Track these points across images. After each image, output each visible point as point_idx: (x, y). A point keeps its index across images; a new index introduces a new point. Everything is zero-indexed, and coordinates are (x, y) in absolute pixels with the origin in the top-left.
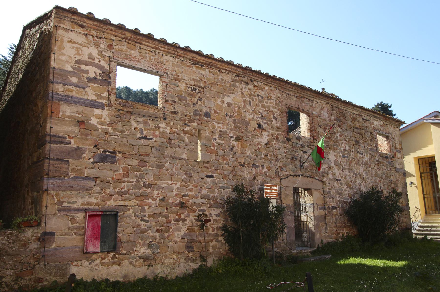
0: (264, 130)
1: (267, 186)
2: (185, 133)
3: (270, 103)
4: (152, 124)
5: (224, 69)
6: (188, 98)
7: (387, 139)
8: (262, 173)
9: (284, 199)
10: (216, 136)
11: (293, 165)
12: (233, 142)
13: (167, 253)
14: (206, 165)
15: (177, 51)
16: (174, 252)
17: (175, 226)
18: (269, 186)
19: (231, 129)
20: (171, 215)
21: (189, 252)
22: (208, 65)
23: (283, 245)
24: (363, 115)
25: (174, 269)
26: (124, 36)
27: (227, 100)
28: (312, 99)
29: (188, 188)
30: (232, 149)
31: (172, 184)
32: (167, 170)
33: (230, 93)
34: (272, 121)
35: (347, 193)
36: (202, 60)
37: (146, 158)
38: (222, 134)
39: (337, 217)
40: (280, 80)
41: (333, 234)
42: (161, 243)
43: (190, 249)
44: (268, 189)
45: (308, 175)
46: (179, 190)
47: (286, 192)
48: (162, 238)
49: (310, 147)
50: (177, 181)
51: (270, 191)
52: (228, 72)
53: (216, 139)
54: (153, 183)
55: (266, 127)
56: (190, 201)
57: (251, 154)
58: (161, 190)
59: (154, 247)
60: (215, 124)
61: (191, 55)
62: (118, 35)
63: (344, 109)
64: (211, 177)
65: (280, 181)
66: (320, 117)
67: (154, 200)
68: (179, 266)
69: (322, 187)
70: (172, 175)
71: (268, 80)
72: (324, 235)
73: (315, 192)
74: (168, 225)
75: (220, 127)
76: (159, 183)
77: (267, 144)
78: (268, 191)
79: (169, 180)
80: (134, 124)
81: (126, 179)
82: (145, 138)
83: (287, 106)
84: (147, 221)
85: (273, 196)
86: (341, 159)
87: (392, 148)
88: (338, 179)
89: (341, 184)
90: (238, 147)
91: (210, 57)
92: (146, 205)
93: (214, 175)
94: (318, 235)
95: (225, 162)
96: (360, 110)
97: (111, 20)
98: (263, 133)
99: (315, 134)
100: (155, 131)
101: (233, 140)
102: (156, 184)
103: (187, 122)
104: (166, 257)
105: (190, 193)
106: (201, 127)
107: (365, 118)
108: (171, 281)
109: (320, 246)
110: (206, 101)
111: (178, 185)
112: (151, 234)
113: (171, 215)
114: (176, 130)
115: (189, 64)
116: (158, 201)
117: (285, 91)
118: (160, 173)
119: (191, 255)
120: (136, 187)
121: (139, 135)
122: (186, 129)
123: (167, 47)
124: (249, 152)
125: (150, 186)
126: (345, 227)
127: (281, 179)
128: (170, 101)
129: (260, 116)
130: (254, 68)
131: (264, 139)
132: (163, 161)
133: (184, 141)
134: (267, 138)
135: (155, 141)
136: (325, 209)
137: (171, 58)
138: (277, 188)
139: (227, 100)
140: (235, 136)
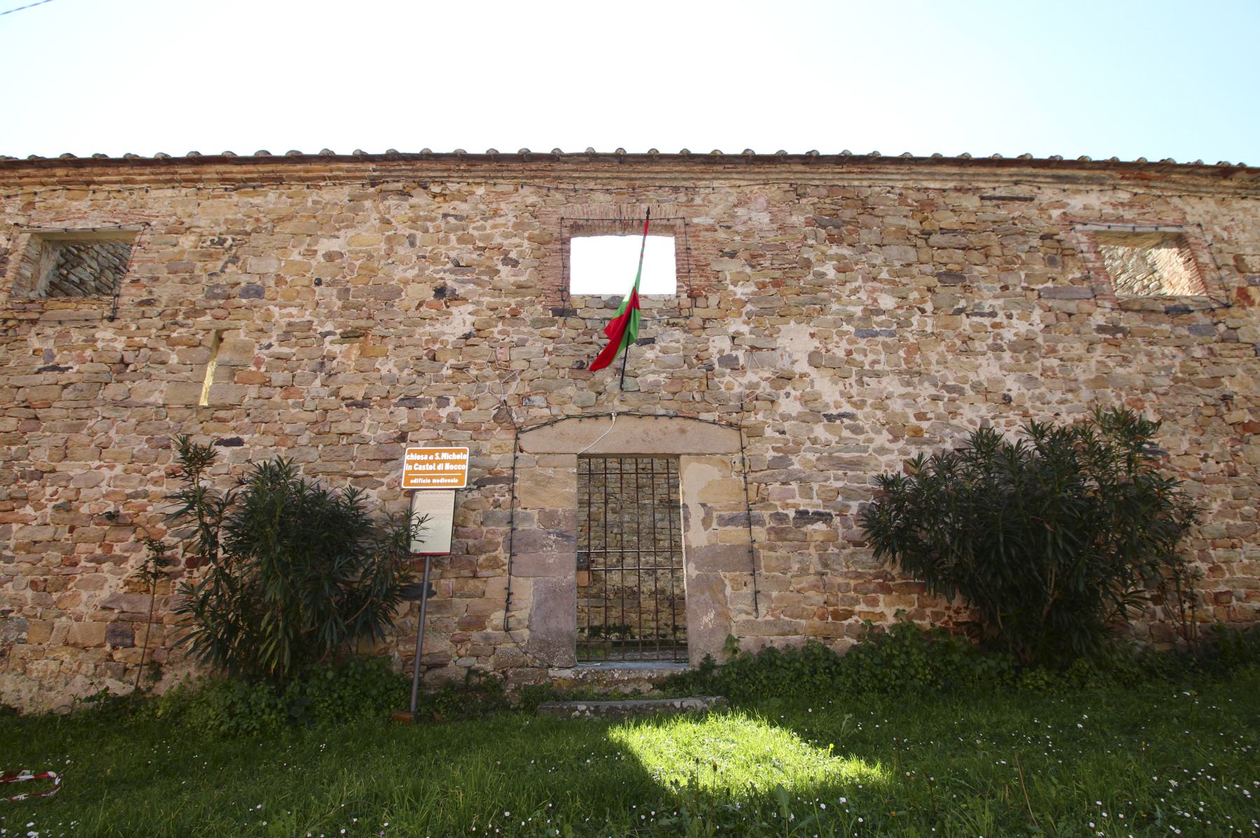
0: (456, 298)
2: (172, 343)
3: (494, 227)
4: (77, 337)
5: (324, 179)
6: (199, 264)
7: (1179, 247)
9: (529, 492)
10: (270, 337)
12: (330, 347)
13: (45, 645)
14: (222, 414)
15: (176, 173)
16: (66, 644)
17: (86, 575)
19: (331, 315)
21: (114, 647)
22: (274, 179)
24: (982, 185)
25: (51, 689)
26: (55, 179)
27: (325, 245)
28: (689, 184)
29: (149, 476)
30: (322, 364)
31: (99, 467)
33: (338, 230)
34: (498, 272)
35: (891, 459)
36: (246, 173)
37: (41, 413)
39: (832, 550)
41: (808, 617)
42: (35, 616)
43: (119, 640)
44: (422, 462)
45: (662, 412)
46: (119, 483)
48: (39, 605)
49: (674, 325)
50: (116, 460)
51: (431, 467)
52: (337, 180)
53: (270, 346)
54: (44, 469)
56: (150, 508)
57: (395, 371)
58: (63, 483)
59: (11, 625)
61: (211, 171)
62: (44, 179)
63: (865, 183)
65: (517, 438)
67: (38, 506)
68: (67, 684)
70: (102, 447)
79: (92, 459)
80: (35, 343)
82: (55, 368)
85: (442, 481)
86: (851, 342)
87: (1211, 275)
88: (834, 412)
89: (857, 430)
91: (263, 159)
92: (16, 521)
93: (246, 438)
94: (708, 619)
95: (290, 401)
96: (954, 170)
98: (453, 310)
99: (697, 282)
100: (83, 349)
101: (332, 342)
102: (53, 471)
103: (180, 318)
104: (39, 654)
105: (151, 488)
106: (223, 324)
107: (990, 193)
108: (31, 719)
109: (720, 659)
110: (252, 261)
111: (119, 469)
112: (11, 592)
114: (145, 340)
115: (218, 192)
116: (49, 510)
118: (69, 444)
119: (118, 655)
121: (40, 364)
122: (174, 335)
123: (148, 170)
124: (391, 365)
125: (39, 475)
126: (886, 590)
127: (519, 430)
128: (144, 281)
129: (450, 266)
131: (460, 320)
135: (78, 372)
136: (749, 521)
137: (169, 192)
139: (325, 245)
140: (339, 331)
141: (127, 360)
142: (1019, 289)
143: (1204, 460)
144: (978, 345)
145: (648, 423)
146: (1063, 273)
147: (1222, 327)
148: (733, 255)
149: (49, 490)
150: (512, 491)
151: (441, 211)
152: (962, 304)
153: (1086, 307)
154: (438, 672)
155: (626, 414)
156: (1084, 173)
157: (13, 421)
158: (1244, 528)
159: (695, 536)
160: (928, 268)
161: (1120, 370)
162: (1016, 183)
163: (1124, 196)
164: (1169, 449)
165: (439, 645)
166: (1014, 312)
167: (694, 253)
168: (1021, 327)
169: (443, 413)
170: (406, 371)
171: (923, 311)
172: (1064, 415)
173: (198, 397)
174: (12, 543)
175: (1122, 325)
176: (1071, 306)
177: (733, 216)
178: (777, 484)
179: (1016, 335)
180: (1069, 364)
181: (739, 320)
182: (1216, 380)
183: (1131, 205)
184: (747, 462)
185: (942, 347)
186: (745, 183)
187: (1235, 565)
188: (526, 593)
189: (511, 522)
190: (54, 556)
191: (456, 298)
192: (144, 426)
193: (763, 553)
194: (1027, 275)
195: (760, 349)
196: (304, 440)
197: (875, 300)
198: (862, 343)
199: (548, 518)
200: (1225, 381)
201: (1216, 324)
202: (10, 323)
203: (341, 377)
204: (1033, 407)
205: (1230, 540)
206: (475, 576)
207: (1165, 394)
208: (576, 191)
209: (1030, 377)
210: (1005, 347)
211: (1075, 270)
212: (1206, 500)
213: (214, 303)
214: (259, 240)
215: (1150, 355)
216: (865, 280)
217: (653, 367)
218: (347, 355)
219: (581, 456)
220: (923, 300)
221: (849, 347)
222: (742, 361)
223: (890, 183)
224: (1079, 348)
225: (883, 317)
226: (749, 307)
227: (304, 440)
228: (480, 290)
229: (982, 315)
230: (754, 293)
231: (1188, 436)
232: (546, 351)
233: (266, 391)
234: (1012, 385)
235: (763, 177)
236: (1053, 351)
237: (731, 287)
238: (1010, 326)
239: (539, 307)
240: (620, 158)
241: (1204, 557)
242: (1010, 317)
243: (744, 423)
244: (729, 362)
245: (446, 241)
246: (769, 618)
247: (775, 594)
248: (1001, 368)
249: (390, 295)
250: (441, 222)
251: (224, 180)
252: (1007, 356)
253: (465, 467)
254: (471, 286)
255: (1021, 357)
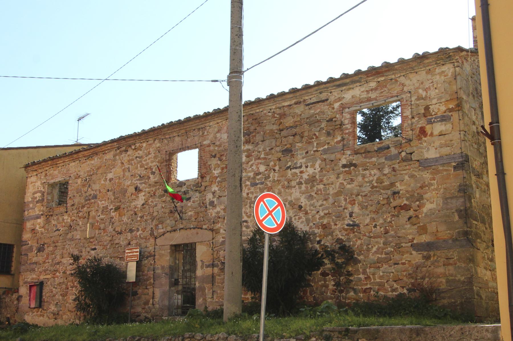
0: (140, 191)
1: (129, 249)
8: (136, 237)
11: (172, 218)
18: (131, 249)
19: (112, 202)
20: (69, 284)
23: (153, 310)
24: (306, 98)
27: (110, 176)
28: (202, 126)
32: (67, 250)
37: (57, 244)
38: (105, 209)
40: (153, 130)
44: (129, 253)
45: (192, 226)
47: (161, 252)
51: (131, 254)
52: (110, 150)
55: (144, 187)
60: (99, 202)
64: (95, 249)
65: (155, 241)
66: (214, 144)
67: (60, 273)
69: (211, 237)
71: (142, 137)
72: (210, 300)
73: (199, 246)
74: (67, 290)
75: (103, 204)
76: (63, 260)
77: (143, 205)
78: (129, 255)
81: (47, 261)
83: (168, 153)
84: (56, 288)
86: (249, 189)
90: (116, 217)
93: (97, 247)
97: (198, 114)
104: (64, 313)
113: (69, 284)
117: (167, 137)
120: (51, 265)
125: (58, 263)
127: (156, 238)
129: (138, 177)
130: (147, 128)
131: (141, 198)
132: (65, 243)
133: (79, 225)
134: (143, 198)
138: (136, 250)
141: (72, 225)
142: (312, 152)
143: (375, 226)
144: (293, 183)
145: (188, 232)
146: (333, 140)
147: (403, 154)
148: (215, 157)
149: (61, 267)
150: (154, 259)
151: (135, 156)
152: (289, 164)
153: (339, 156)
154: (139, 317)
155: (182, 229)
156: (348, 81)
157: (52, 247)
158: (386, 258)
159: (199, 272)
160: (278, 149)
161: (349, 186)
162: (321, 93)
163: (373, 84)
164: (360, 223)
165: (139, 309)
166: (309, 164)
167: (203, 158)
168: (310, 171)
169: (138, 234)
170: (130, 220)
171: (274, 170)
172: (321, 212)
173: (86, 235)
174: (56, 283)
175: (354, 162)
176: (332, 157)
177: (216, 138)
178: (222, 251)
179: (308, 175)
180: (327, 186)
181: (215, 185)
182: (392, 184)
183: (376, 89)
184: (214, 243)
185: (280, 187)
186: (220, 121)
187: (376, 276)
188: (158, 293)
189: (154, 270)
190: (64, 286)
191: (140, 191)
192: (76, 246)
193: (217, 277)
194: (317, 144)
195: (221, 197)
196: (108, 247)
197: (258, 168)
198: (252, 189)
199: (163, 268)
200: (398, 184)
201: (401, 153)
202: (48, 216)
203: (115, 224)
204: (310, 210)
205: (377, 264)
206: (147, 289)
207: (365, 196)
208: (170, 138)
209: (311, 196)
210: (303, 182)
211: (338, 136)
212: (370, 247)
213: (87, 203)
214: (94, 177)
215: (364, 176)
216: (255, 160)
217: (190, 209)
218: (116, 215)
219: (172, 246)
220: (275, 165)
221: (248, 192)
222: (215, 203)
223: (270, 108)
224: (333, 177)
225: (260, 176)
226: (218, 179)
227: (108, 247)
228: (146, 186)
229: (296, 168)
230: (220, 173)
231: (370, 216)
232: (162, 207)
233: (100, 231)
234: (303, 201)
235: (225, 117)
236: (321, 181)
237: (214, 171)
238: (307, 171)
239: (160, 190)
240: (179, 122)
241: (364, 272)
242: (307, 167)
243: (214, 228)
244: (212, 203)
245: (137, 168)
246: (217, 300)
247: (219, 292)
248: (300, 193)
249: (124, 192)
250: (135, 160)
251: (85, 157)
252: (303, 187)
253: (138, 254)
254: (143, 185)
255: (309, 186)
